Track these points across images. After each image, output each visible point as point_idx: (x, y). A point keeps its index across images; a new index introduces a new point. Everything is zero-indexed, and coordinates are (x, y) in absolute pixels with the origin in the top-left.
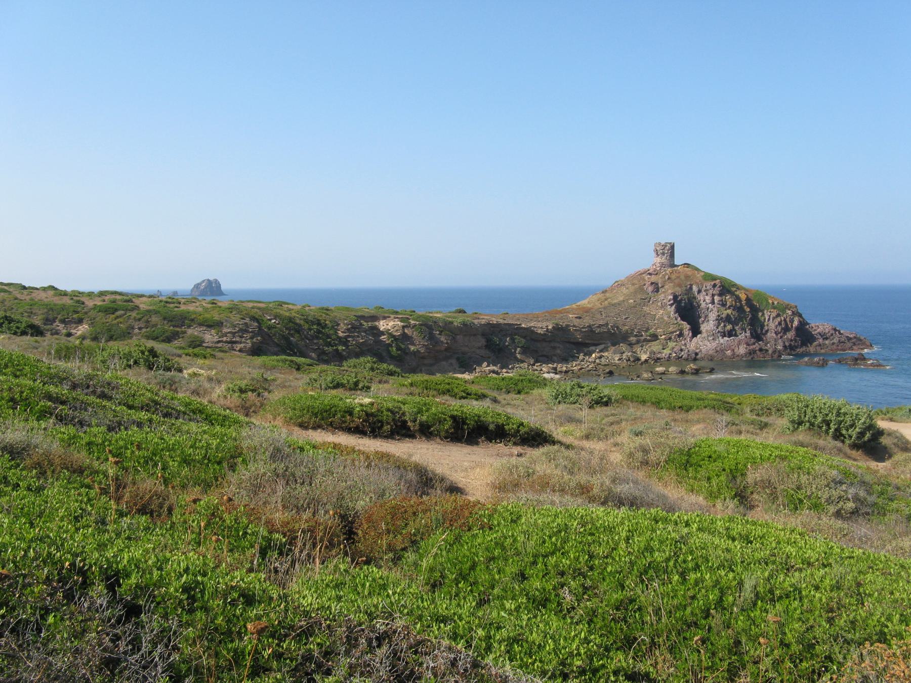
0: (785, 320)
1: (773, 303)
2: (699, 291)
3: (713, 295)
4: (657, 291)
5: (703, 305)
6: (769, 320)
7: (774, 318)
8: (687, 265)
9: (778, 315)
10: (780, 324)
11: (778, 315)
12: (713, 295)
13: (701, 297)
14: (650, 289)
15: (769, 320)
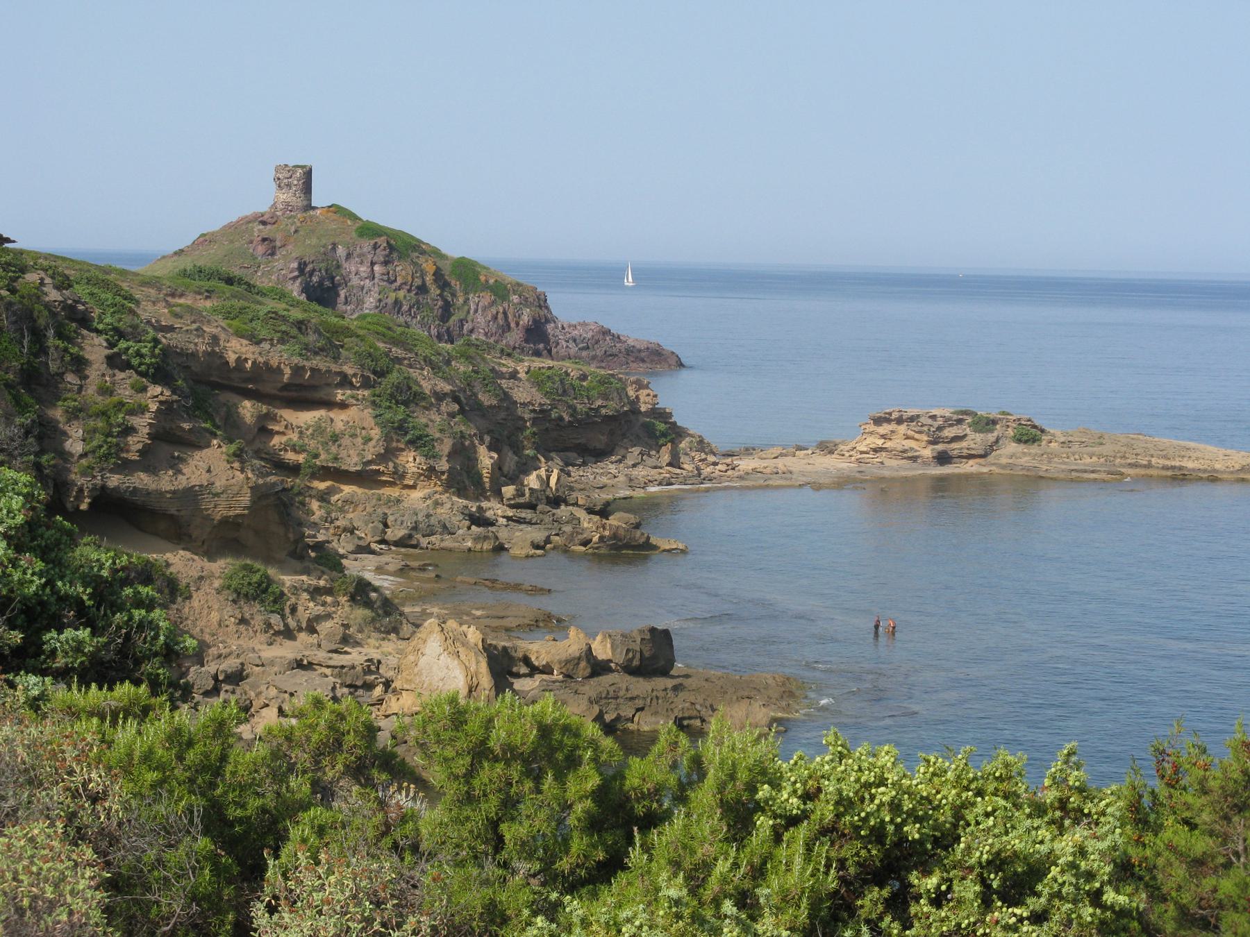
0: (505, 313)
1: (487, 281)
2: (349, 256)
3: (373, 264)
4: (273, 254)
5: (355, 281)
6: (476, 311)
7: (485, 309)
8: (336, 209)
9: (493, 303)
10: (495, 318)
11: (493, 303)
12: (373, 264)
13: (350, 267)
14: (261, 249)
15: (476, 311)
